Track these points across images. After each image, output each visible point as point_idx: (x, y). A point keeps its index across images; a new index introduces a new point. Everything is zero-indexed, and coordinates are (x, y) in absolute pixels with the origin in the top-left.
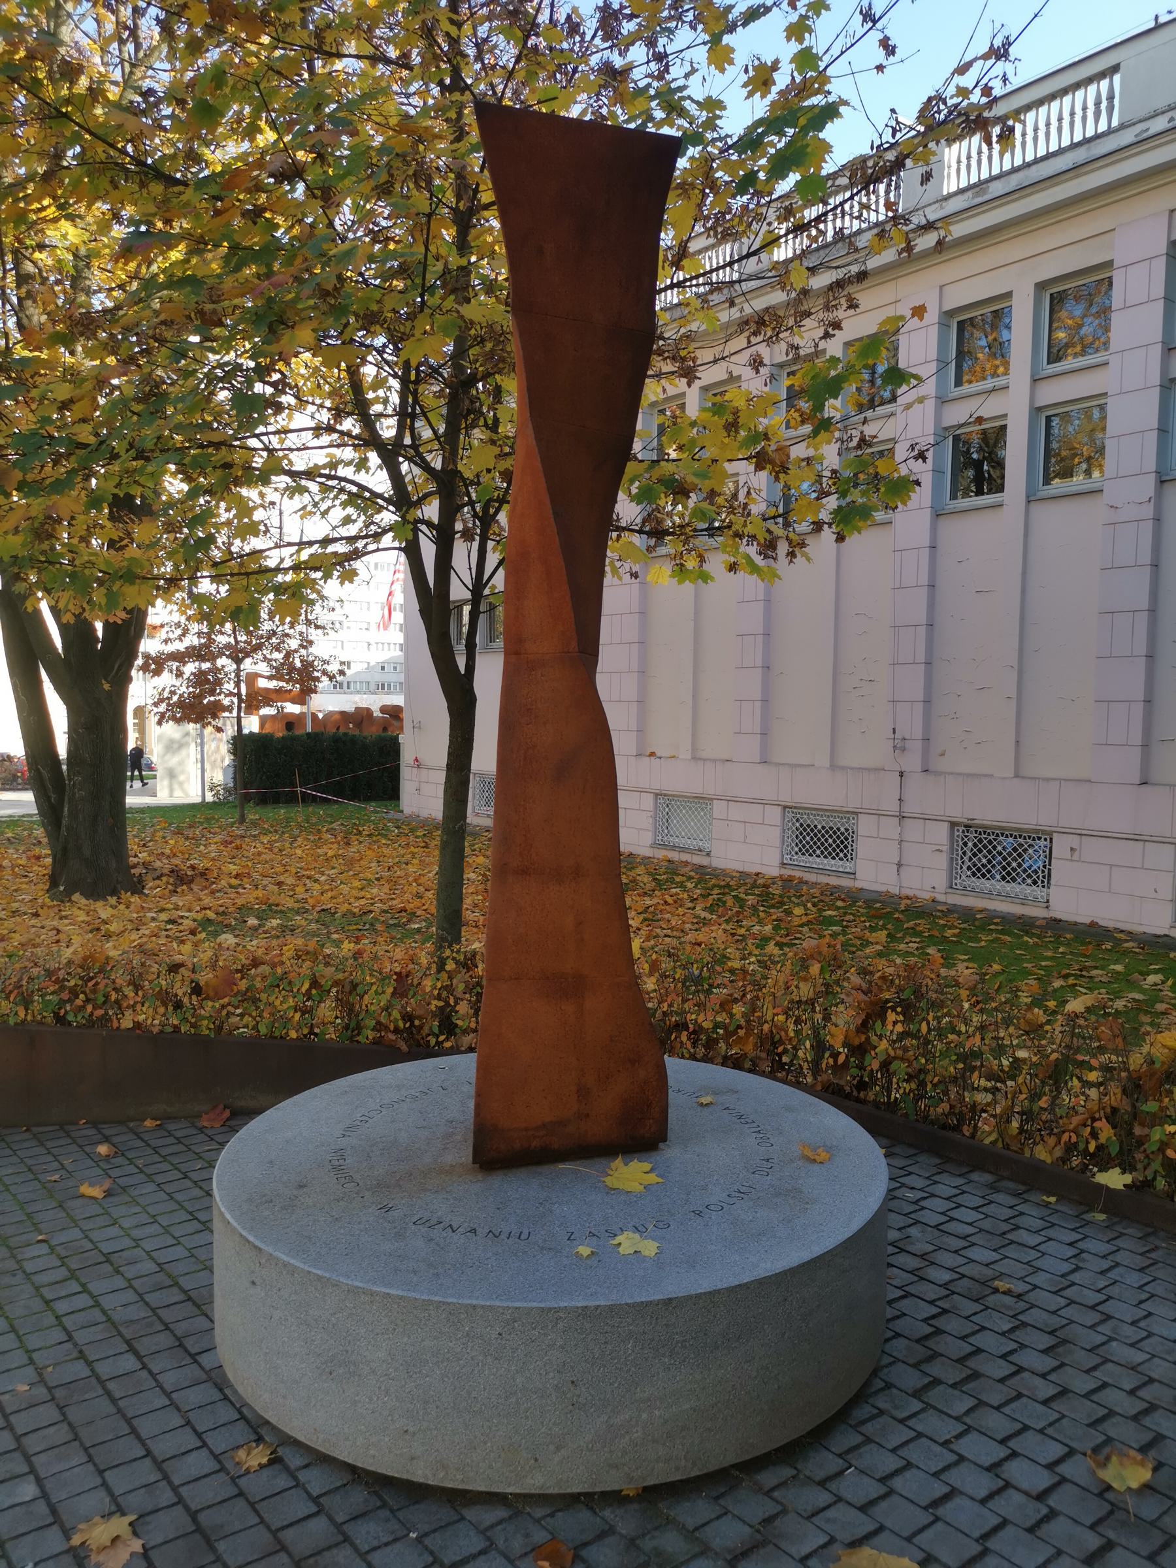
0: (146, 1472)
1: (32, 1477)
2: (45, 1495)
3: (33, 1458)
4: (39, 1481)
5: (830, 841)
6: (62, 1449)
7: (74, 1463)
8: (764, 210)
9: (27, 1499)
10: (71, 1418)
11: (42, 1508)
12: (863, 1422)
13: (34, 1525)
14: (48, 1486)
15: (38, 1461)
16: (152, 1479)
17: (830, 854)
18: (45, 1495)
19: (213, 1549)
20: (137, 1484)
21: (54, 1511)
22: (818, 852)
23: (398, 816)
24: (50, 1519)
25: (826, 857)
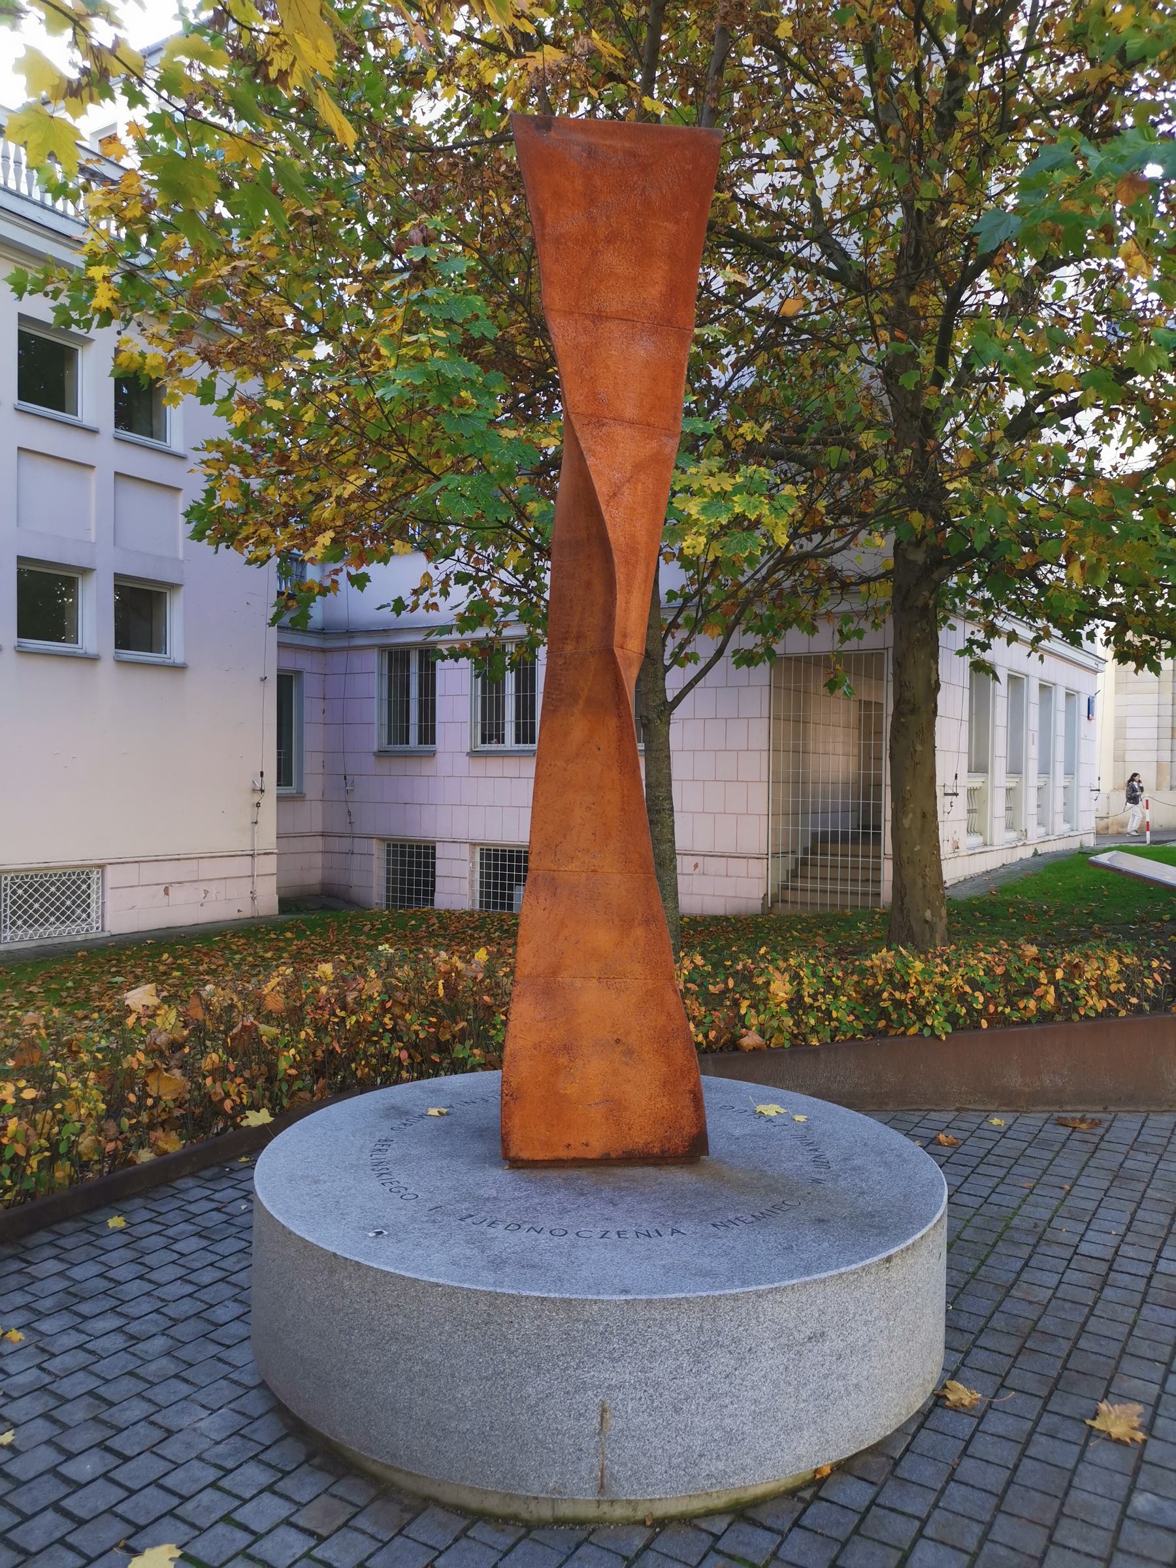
0: (1041, 1446)
1: (1129, 1512)
2: (1132, 1489)
3: (1113, 1528)
4: (1127, 1503)
5: (36, 906)
6: (1082, 1515)
7: (1086, 1495)
8: (1080, 313)
9: (1149, 1495)
10: (1043, 1542)
11: (1142, 1480)
12: (864, 8)
13: (1159, 1471)
14: (1121, 1493)
15: (1109, 1522)
16: (1043, 1439)
17: (84, 901)
18: (1132, 1489)
19: (1060, 1376)
20: (1057, 1443)
21: (1136, 1472)
22: (84, 887)
23: (95, 323)
24: (1145, 1467)
25: (88, 906)
